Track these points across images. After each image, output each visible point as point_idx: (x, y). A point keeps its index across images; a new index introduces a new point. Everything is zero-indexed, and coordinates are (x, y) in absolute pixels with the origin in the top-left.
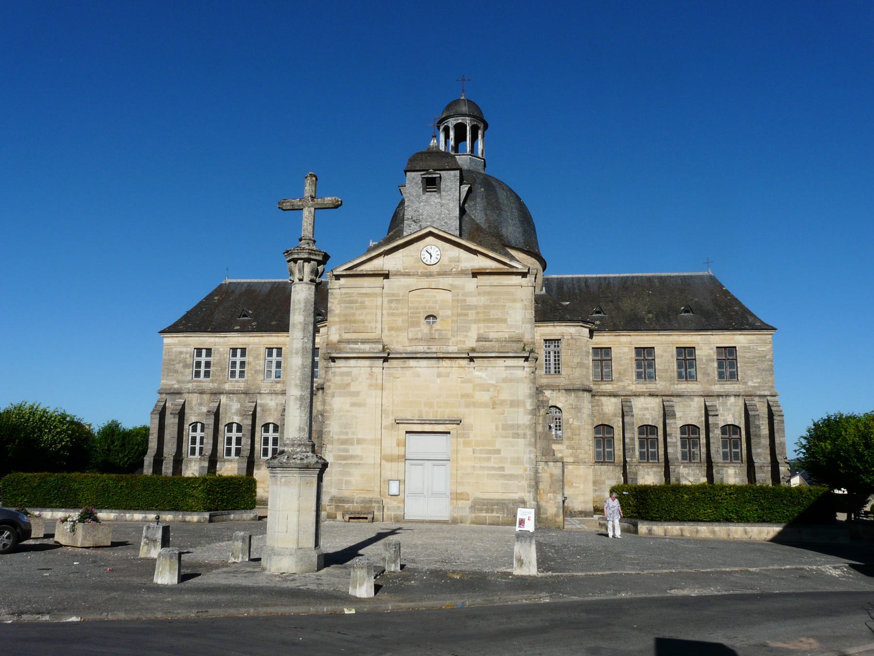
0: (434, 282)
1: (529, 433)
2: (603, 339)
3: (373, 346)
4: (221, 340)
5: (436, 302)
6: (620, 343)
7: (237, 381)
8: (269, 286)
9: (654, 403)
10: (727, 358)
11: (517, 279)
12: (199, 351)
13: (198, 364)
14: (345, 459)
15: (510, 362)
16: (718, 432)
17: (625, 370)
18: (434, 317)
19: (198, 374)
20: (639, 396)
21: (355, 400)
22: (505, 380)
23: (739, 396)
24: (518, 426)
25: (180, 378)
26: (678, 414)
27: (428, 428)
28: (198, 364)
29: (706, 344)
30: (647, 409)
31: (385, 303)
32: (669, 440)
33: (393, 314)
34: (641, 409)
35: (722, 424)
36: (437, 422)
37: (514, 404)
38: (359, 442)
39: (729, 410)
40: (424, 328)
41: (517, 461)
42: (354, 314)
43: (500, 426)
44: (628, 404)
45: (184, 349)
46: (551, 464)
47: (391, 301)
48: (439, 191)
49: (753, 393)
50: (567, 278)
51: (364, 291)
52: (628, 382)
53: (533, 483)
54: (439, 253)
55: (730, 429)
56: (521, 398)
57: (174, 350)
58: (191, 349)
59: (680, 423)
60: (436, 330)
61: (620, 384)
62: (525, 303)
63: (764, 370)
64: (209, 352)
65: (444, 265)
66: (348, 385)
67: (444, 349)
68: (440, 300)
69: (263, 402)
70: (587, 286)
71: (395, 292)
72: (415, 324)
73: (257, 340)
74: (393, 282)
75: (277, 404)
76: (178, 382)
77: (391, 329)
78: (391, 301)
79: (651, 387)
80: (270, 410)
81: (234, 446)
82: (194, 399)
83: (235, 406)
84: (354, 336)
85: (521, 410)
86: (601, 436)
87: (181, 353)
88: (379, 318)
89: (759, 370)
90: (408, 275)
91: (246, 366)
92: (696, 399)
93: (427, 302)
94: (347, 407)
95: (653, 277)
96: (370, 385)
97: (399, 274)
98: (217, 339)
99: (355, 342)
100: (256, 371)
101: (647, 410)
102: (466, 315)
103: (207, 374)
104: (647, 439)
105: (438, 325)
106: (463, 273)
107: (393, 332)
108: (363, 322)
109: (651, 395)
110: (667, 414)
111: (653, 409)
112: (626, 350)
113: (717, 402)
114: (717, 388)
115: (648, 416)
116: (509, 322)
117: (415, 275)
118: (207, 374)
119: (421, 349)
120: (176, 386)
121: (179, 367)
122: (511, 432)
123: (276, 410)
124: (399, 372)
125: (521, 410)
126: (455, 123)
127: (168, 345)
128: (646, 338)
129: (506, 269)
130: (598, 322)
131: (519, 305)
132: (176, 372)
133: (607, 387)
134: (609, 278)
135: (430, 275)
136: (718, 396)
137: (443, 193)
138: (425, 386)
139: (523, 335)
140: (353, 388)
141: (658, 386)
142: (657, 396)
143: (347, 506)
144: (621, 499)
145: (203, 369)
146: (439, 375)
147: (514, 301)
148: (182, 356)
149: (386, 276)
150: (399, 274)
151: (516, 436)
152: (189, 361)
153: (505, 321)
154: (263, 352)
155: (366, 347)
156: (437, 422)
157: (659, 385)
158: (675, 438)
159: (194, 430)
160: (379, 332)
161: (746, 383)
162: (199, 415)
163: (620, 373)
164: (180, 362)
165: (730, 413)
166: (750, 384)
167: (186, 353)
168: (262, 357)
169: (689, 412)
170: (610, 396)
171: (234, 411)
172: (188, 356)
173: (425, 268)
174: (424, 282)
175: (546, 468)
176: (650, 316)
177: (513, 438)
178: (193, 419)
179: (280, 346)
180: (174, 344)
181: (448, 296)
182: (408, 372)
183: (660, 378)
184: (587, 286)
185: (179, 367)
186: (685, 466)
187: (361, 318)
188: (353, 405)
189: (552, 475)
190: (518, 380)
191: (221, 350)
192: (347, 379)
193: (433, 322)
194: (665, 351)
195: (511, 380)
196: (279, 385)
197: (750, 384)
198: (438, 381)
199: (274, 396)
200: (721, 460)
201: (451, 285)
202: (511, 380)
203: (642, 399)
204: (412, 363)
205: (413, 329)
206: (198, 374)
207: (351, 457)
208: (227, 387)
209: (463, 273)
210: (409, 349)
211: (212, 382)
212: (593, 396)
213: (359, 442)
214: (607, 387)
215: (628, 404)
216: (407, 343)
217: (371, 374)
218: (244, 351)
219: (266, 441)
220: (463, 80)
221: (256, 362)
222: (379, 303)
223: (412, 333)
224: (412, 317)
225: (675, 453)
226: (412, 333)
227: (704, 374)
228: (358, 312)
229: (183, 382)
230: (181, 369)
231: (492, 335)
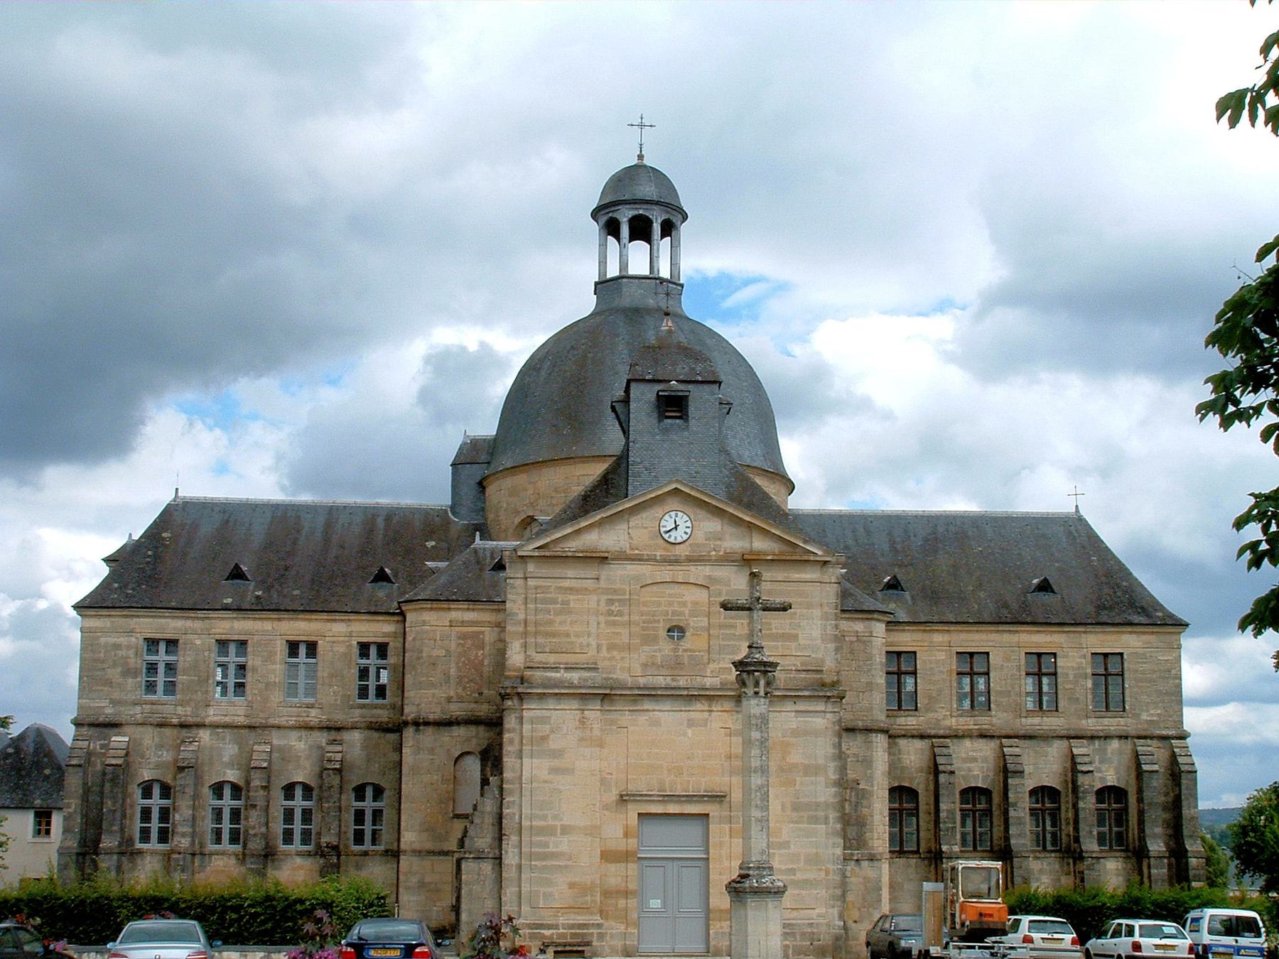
0: (680, 573)
1: (833, 815)
2: (906, 640)
3: (586, 674)
4: (197, 625)
5: (684, 604)
6: (932, 645)
7: (233, 704)
9: (986, 749)
10: (1109, 670)
12: (152, 643)
13: (152, 668)
14: (544, 859)
15: (801, 706)
16: (1091, 799)
17: (940, 691)
18: (682, 630)
19: (151, 687)
20: (963, 737)
21: (556, 763)
22: (796, 733)
23: (1126, 738)
24: (818, 805)
25: (116, 695)
26: (1028, 769)
27: (673, 809)
28: (152, 668)
29: (1075, 652)
30: (975, 760)
31: (603, 604)
32: (1012, 813)
33: (614, 624)
34: (965, 760)
35: (1098, 786)
36: (690, 799)
38: (566, 830)
40: (665, 648)
41: (814, 860)
42: (551, 623)
43: (788, 805)
44: (945, 751)
45: (122, 640)
46: (865, 864)
48: (684, 416)
49: (1148, 733)
51: (567, 583)
52: (944, 712)
53: (839, 892)
54: (689, 524)
55: (1110, 794)
56: (821, 761)
57: (103, 640)
58: (137, 640)
59: (1031, 784)
60: (685, 651)
61: (931, 715)
62: (826, 609)
63: (1167, 694)
64: (172, 644)
65: (698, 545)
66: (544, 738)
70: (868, 533)
71: (618, 586)
72: (649, 640)
73: (268, 626)
74: (619, 573)
75: (311, 747)
76: (114, 702)
77: (611, 647)
78: (610, 602)
79: (984, 722)
81: (226, 826)
82: (149, 737)
83: (230, 750)
84: (552, 659)
85: (821, 779)
86: (897, 805)
87: (117, 647)
88: (593, 630)
89: (1159, 693)
90: (638, 559)
91: (249, 675)
93: (671, 604)
94: (543, 774)
96: (582, 739)
97: (623, 557)
98: (189, 623)
99: (556, 669)
100: (267, 684)
101: (973, 763)
102: (733, 626)
103: (170, 688)
104: (974, 812)
105: (687, 643)
107: (615, 653)
108: (568, 635)
109: (983, 736)
110: (1006, 771)
111: (985, 760)
112: (942, 656)
114: (1091, 724)
116: (801, 641)
117: (651, 559)
118: (170, 688)
119: (661, 681)
120: (109, 711)
121: (114, 674)
122: (805, 814)
124: (625, 719)
125: (821, 779)
126: (631, 213)
128: (977, 636)
131: (817, 613)
132: (109, 683)
133: (908, 722)
135: (675, 561)
136: (1092, 738)
137: (692, 422)
138: (683, 746)
139: (823, 661)
140: (553, 744)
141: (994, 720)
142: (992, 737)
143: (547, 932)
144: (1269, 913)
145: (161, 678)
146: (691, 723)
147: (809, 606)
148: (120, 653)
150: (623, 557)
151: (813, 820)
152: (133, 662)
153: (796, 637)
154: (281, 649)
155: (575, 676)
156: (690, 799)
157: (998, 719)
158: (1021, 808)
159: (147, 793)
160: (592, 652)
161: (1137, 716)
162: (158, 766)
163: (930, 697)
164: (114, 666)
165: (1108, 768)
166: (1144, 717)
167: (129, 647)
168: (278, 657)
169: (1042, 766)
170: (913, 737)
172: (131, 653)
173: (666, 549)
174: (665, 573)
175: (857, 869)
176: (982, 594)
177: (809, 823)
178: (147, 775)
179: (313, 638)
180: (103, 631)
181: (702, 595)
182: (643, 718)
183: (998, 705)
184: (868, 533)
185: (114, 674)
186: (1036, 858)
187: (563, 628)
188: (555, 771)
190: (815, 733)
191: (198, 642)
192: (544, 729)
193: (680, 638)
194: (1007, 659)
195: (806, 733)
196: (313, 712)
198: (690, 732)
199: (304, 733)
200: (1095, 847)
201: (710, 577)
202: (806, 733)
203: (967, 743)
204: (647, 705)
205: (646, 648)
206: (151, 687)
207: (554, 855)
208: (212, 715)
210: (642, 681)
211: (182, 703)
212: (890, 737)
213: (566, 830)
214: (908, 722)
215: (945, 751)
217: (583, 721)
218: (243, 644)
219: (218, 813)
220: (641, 126)
221: (269, 665)
222: (593, 605)
223: (646, 652)
224: (644, 629)
225: (951, 812)
227: (1070, 699)
228: (558, 619)
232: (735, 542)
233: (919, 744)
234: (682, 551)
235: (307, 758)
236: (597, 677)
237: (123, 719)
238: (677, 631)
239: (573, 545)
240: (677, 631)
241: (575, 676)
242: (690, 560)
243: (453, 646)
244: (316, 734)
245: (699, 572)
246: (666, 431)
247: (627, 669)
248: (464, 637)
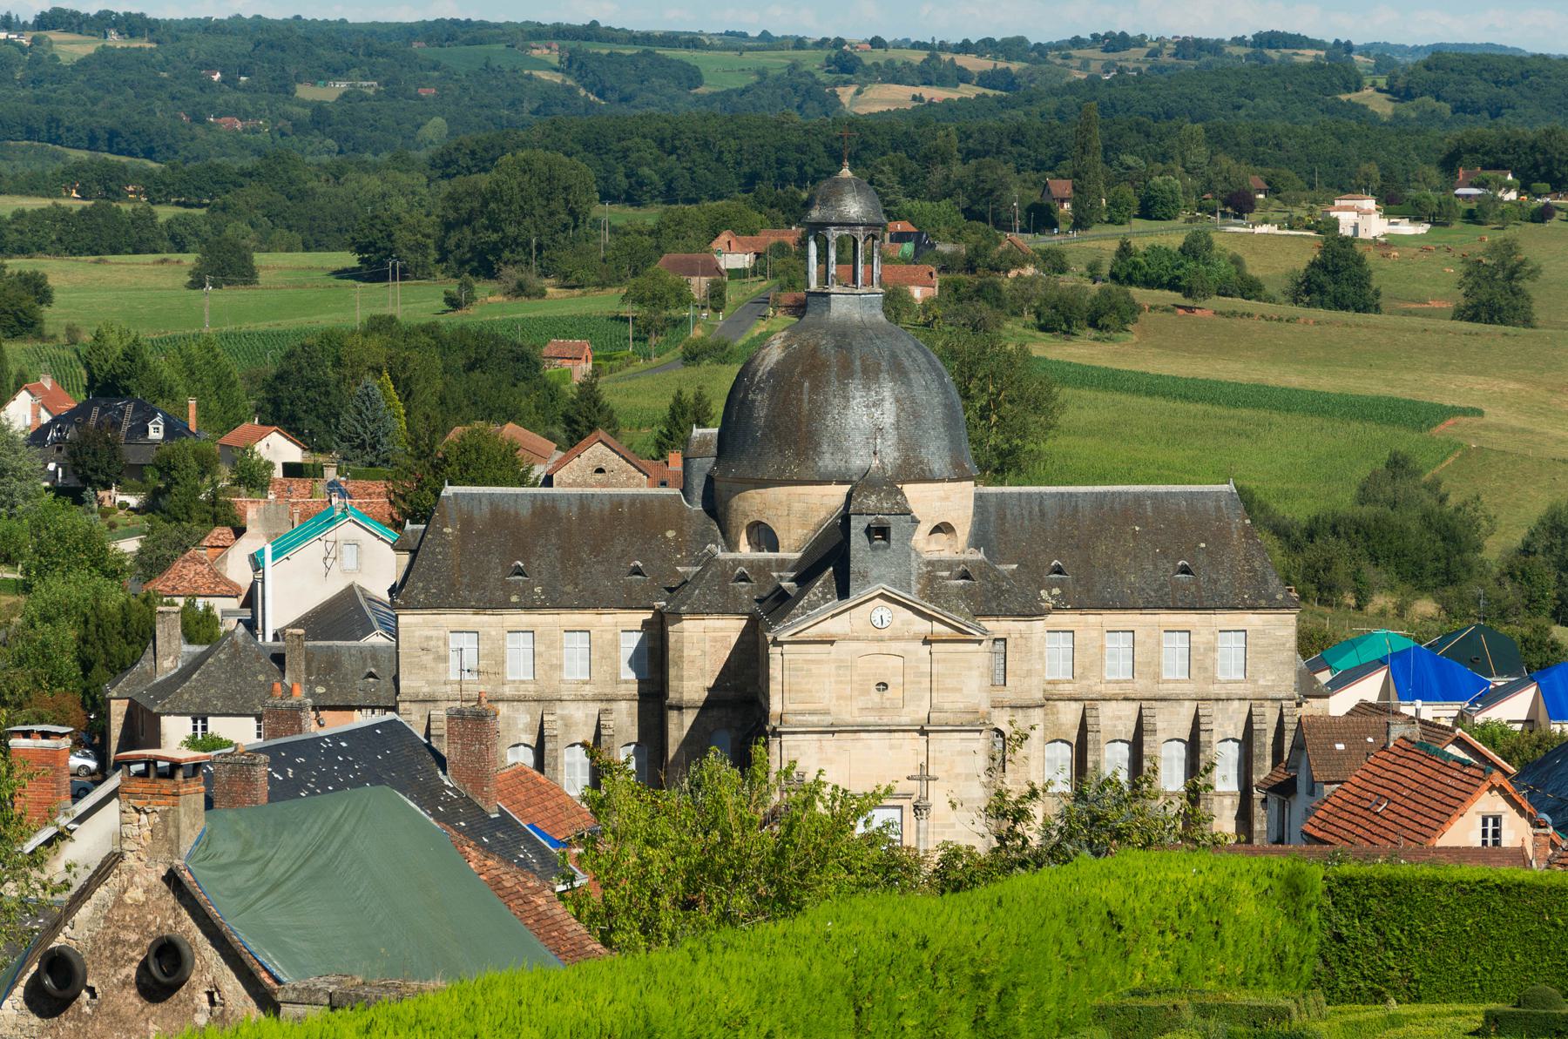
8: (525, 511)
11: (977, 735)
18: (885, 685)
22: (960, 753)
25: (431, 677)
26: (1159, 726)
37: (968, 777)
39: (1231, 718)
40: (876, 696)
47: (839, 668)
50: (1011, 494)
51: (809, 657)
67: (896, 720)
68: (889, 668)
69: (565, 712)
76: (428, 682)
77: (839, 698)
80: (577, 724)
84: (800, 707)
87: (429, 638)
92: (1187, 703)
95: (1144, 493)
97: (845, 638)
105: (887, 694)
106: (914, 638)
109: (1126, 699)
113: (1213, 708)
115: (1120, 728)
120: (426, 689)
123: (586, 724)
127: (408, 625)
129: (962, 637)
130: (1056, 591)
131: (975, 673)
134: (1076, 495)
147: (970, 669)
149: (832, 642)
150: (845, 638)
155: (815, 719)
166: (1261, 682)
167: (438, 639)
171: (521, 726)
182: (859, 744)
189: (671, 170)
196: (587, 687)
197: (1261, 682)
204: (863, 735)
209: (914, 638)
210: (859, 720)
216: (856, 713)
217: (821, 748)
223: (861, 702)
226: (861, 702)
229: (435, 683)
230: (431, 664)
231: (947, 706)
232: (924, 626)
233: (1074, 705)
234: (886, 633)
235: (586, 724)
236: (828, 719)
237: (439, 696)
238: (883, 686)
239: (812, 633)
240: (883, 686)
241: (815, 719)
242: (891, 639)
243: (708, 645)
244: (591, 704)
245: (896, 647)
246: (875, 549)
247: (850, 714)
248: (715, 640)
